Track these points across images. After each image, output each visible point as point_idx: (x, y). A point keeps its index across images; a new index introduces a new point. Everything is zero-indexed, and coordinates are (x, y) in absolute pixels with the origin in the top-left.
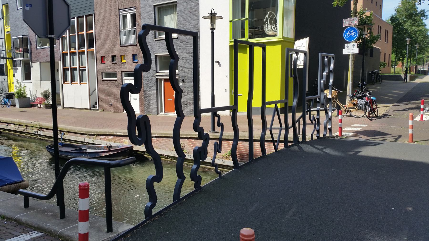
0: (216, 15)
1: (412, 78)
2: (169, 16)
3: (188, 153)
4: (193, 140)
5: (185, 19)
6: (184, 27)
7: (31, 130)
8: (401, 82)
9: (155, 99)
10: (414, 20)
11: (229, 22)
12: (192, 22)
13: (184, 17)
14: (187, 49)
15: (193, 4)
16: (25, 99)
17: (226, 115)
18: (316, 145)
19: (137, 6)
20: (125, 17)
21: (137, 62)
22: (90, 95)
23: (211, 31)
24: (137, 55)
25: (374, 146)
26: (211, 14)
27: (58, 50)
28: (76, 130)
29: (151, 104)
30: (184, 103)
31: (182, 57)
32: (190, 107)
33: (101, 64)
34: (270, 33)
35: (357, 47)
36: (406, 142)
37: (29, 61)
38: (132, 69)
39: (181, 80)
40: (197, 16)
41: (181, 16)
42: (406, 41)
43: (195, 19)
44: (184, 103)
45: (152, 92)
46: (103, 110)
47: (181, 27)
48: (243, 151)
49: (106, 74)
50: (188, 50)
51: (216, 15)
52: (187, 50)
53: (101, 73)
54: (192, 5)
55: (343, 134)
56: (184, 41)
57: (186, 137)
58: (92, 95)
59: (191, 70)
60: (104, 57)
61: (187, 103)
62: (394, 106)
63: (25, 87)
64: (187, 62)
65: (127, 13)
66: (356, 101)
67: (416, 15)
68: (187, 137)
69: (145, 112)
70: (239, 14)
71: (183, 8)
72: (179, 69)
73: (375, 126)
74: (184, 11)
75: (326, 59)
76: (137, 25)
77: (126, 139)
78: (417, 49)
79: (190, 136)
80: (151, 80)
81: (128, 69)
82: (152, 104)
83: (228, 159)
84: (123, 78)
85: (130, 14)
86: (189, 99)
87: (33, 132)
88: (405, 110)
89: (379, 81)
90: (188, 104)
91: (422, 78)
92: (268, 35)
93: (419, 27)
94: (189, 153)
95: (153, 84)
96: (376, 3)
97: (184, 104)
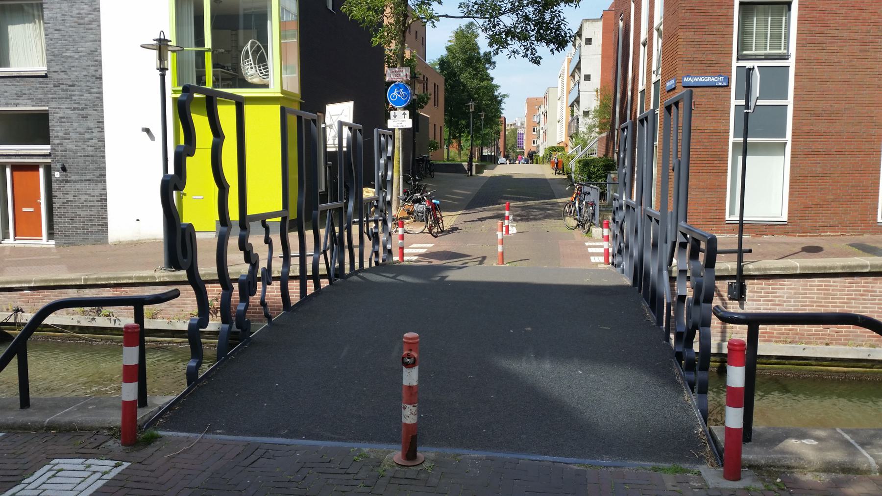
0: (169, 43)
1: (480, 169)
2: (21, 26)
3: (111, 315)
5: (66, 37)
8: (463, 175)
10: (476, 69)
14: (71, 101)
18: (383, 272)
23: (160, 73)
25: (458, 270)
26: (160, 40)
31: (60, 118)
32: (83, 225)
34: (256, 80)
35: (410, 118)
36: (495, 265)
39: (59, 166)
40: (95, 33)
41: (56, 30)
42: (469, 106)
43: (92, 39)
47: (57, 52)
50: (75, 103)
51: (169, 43)
52: (72, 102)
54: (83, 9)
55: (405, 258)
56: (63, 84)
62: (463, 214)
64: (73, 127)
66: (412, 207)
67: (479, 60)
68: (109, 284)
70: (190, 40)
71: (60, 14)
72: (53, 142)
73: (445, 244)
74: (63, 20)
75: (382, 139)
78: (472, 112)
86: (78, 208)
88: (481, 220)
89: (430, 174)
90: (76, 217)
91: (493, 169)
92: (251, 83)
93: (483, 82)
94: (113, 316)
96: (416, 32)
97: (65, 220)
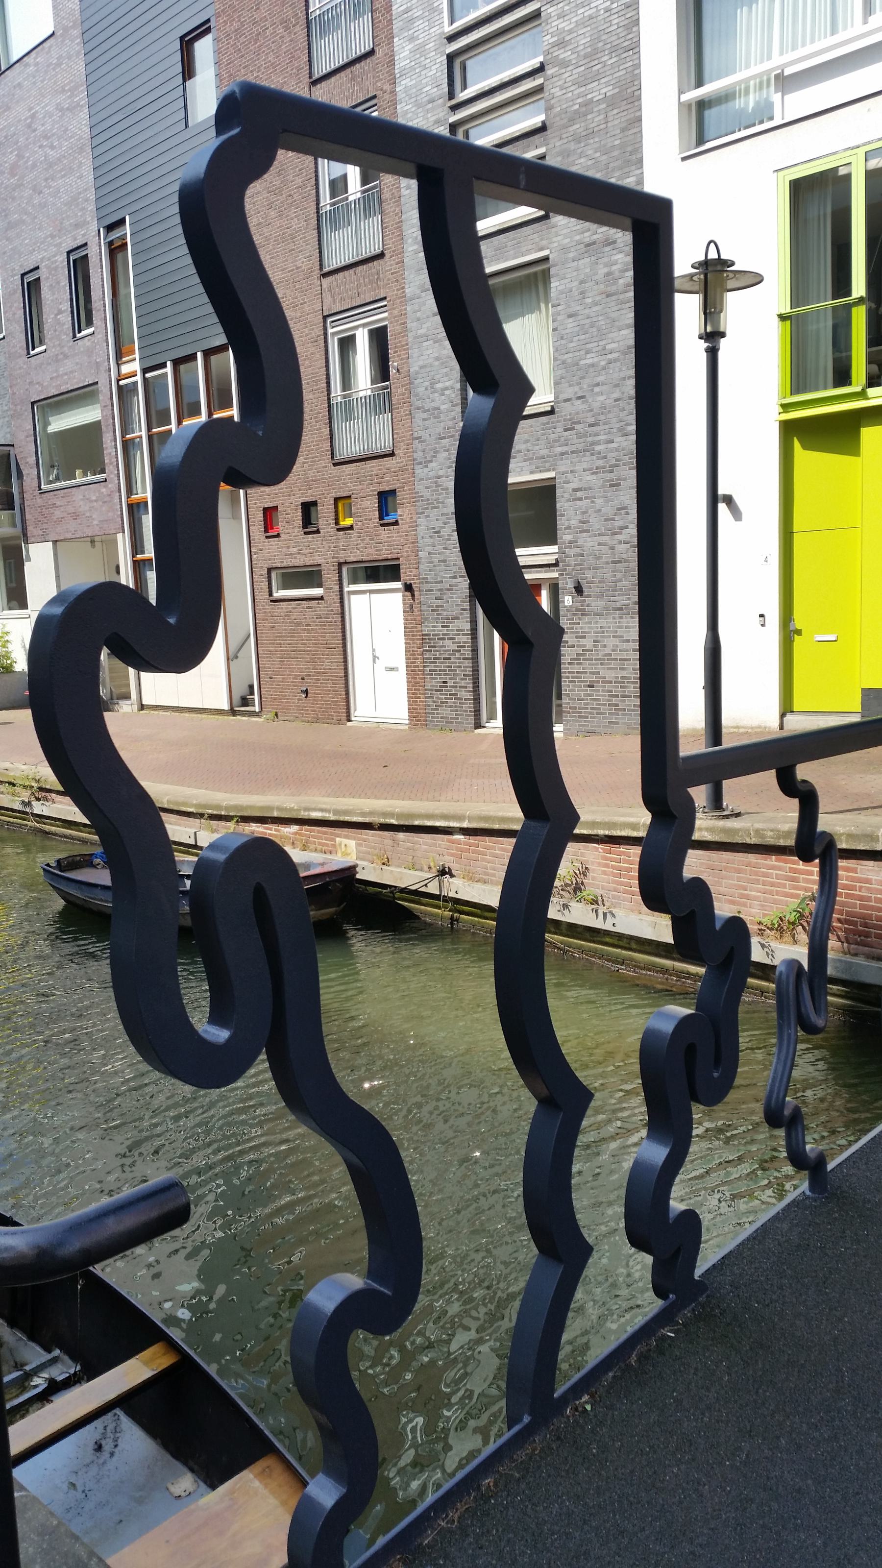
2: (519, 321)
3: (600, 902)
4: (622, 849)
5: (586, 326)
6: (582, 362)
7: (10, 797)
9: (467, 667)
11: (777, 319)
12: (615, 334)
13: (580, 317)
14: (592, 455)
15: (620, 261)
16: (6, 677)
17: (765, 728)
19: (391, 294)
20: (347, 344)
21: (397, 521)
22: (228, 659)
23: (707, 344)
24: (393, 492)
27: (112, 492)
28: (165, 801)
29: (451, 687)
30: (582, 681)
31: (575, 490)
33: (263, 538)
37: (18, 538)
38: (377, 550)
39: (570, 585)
44: (582, 681)
45: (454, 639)
46: (276, 715)
48: (862, 907)
49: (284, 575)
50: (598, 459)
52: (594, 457)
53: (266, 571)
56: (579, 423)
57: (590, 832)
58: (237, 657)
59: (610, 542)
60: (275, 508)
61: (594, 681)
63: (7, 633)
65: (356, 328)
69: (431, 721)
76: (393, 371)
77: (346, 837)
79: (609, 830)
80: (448, 590)
81: (361, 552)
82: (456, 687)
83: (787, 937)
84: (346, 589)
85: (366, 331)
86: (602, 664)
87: (17, 806)
90: (598, 682)
95: (457, 605)
